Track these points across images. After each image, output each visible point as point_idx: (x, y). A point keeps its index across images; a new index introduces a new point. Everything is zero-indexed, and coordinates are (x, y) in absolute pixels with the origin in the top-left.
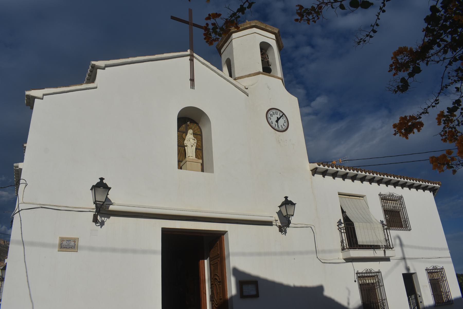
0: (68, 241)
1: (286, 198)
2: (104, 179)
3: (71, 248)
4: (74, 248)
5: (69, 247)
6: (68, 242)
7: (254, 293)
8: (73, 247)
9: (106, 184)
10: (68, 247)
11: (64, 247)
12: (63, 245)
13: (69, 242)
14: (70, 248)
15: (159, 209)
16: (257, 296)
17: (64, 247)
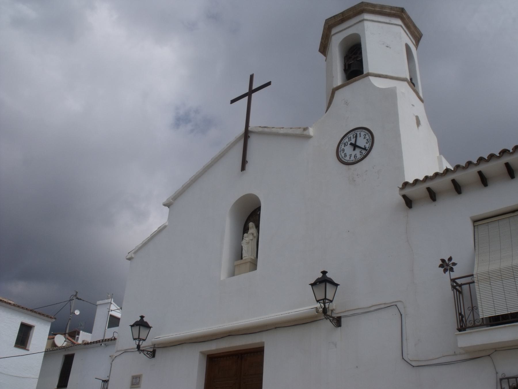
0: (136, 378)
2: (144, 317)
3: (137, 384)
4: (139, 383)
6: (136, 379)
9: (146, 323)
10: (136, 384)
11: (134, 384)
13: (137, 379)
17: (134, 384)
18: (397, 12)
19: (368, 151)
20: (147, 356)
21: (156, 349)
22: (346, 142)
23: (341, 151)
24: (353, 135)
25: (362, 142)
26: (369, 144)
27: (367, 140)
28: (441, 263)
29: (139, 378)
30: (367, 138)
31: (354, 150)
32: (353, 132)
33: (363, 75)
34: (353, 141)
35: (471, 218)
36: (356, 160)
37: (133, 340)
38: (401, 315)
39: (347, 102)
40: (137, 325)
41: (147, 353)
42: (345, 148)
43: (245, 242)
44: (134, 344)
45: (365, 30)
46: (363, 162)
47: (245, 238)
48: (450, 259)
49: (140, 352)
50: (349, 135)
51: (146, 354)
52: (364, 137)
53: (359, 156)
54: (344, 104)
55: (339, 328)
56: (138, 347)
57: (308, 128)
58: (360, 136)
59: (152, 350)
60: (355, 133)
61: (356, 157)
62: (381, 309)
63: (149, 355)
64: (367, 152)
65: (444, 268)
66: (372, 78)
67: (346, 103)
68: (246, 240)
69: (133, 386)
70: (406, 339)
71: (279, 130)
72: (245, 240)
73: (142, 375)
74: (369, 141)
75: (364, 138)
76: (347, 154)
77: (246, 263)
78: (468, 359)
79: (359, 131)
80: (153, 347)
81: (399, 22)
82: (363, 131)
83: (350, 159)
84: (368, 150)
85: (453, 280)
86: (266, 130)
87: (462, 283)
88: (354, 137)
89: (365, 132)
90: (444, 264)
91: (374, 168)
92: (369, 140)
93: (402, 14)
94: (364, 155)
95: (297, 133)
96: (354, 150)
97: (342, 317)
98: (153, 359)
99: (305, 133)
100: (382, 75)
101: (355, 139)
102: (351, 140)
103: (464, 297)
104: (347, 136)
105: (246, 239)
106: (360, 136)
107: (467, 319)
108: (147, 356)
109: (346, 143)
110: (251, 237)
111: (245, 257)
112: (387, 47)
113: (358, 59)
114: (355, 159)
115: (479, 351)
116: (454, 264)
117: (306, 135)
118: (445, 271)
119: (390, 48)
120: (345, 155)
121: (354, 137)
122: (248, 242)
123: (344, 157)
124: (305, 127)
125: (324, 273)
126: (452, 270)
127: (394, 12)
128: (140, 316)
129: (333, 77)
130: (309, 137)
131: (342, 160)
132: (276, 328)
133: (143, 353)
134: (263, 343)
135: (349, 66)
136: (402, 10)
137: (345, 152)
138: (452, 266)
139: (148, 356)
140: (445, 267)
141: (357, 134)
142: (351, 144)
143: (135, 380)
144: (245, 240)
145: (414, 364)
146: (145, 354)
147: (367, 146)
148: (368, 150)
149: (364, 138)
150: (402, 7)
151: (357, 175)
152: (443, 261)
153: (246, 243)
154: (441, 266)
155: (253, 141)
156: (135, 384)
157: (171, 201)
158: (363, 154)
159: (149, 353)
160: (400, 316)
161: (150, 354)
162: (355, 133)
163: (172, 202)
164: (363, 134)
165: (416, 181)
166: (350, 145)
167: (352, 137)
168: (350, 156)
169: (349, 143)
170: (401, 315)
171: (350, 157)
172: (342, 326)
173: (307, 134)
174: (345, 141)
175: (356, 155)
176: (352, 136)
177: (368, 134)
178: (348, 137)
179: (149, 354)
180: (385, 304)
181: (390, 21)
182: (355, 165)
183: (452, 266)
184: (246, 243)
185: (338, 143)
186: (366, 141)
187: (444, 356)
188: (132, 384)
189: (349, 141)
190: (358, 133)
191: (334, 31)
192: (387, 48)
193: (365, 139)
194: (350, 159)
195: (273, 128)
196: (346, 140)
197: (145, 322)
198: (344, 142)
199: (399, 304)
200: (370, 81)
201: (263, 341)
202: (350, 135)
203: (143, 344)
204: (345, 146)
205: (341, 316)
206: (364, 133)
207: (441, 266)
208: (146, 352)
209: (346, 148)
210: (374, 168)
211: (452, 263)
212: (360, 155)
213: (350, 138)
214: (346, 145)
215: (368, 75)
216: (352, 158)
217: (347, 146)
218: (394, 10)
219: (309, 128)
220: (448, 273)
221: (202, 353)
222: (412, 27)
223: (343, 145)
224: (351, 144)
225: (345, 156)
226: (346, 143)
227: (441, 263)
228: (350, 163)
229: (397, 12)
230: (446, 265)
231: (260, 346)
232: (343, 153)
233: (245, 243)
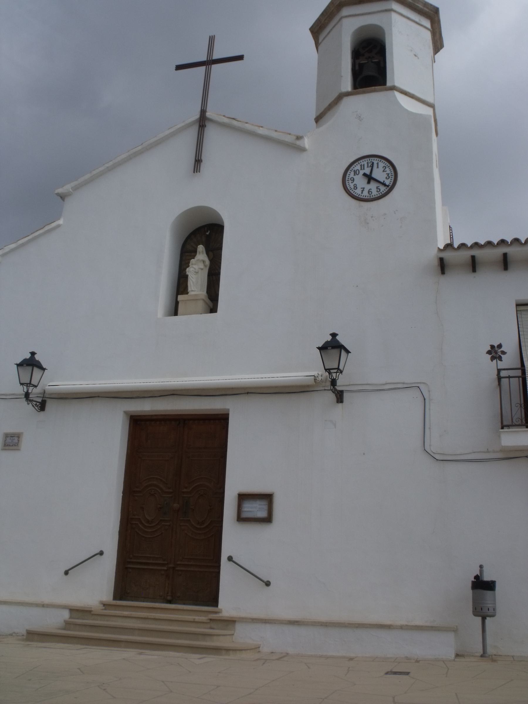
0: (12, 437)
1: (33, 354)
2: (36, 353)
3: (15, 445)
4: (17, 445)
5: (13, 444)
6: (12, 438)
7: (263, 514)
8: (16, 444)
9: (38, 362)
10: (11, 444)
11: (8, 445)
12: (6, 443)
13: (13, 438)
14: (13, 446)
15: (38, 396)
16: (268, 519)
17: (8, 445)
18: (430, 12)
19: (391, 188)
20: (35, 408)
21: (45, 399)
22: (357, 170)
23: (350, 179)
24: (368, 163)
25: (379, 174)
26: (389, 180)
27: (388, 174)
28: (489, 348)
29: (19, 437)
30: (387, 172)
31: (369, 182)
32: (368, 159)
33: (385, 86)
34: (367, 171)
35: (516, 301)
36: (370, 197)
37: (20, 385)
38: (425, 399)
39: (360, 117)
40: (28, 365)
41: (36, 405)
42: (355, 177)
43: (193, 271)
44: (21, 390)
45: (393, 26)
46: (381, 201)
47: (192, 264)
48: (500, 346)
49: (29, 403)
50: (361, 161)
51: (34, 405)
52: (383, 169)
53: (375, 193)
54: (356, 118)
55: (340, 404)
56: (27, 395)
57: (303, 137)
58: (378, 167)
59: (40, 400)
60: (371, 161)
61: (370, 193)
62: (399, 388)
63: (38, 408)
64: (388, 188)
65: (491, 355)
66: (397, 94)
67: (359, 118)
68: (195, 269)
69: (7, 448)
70: (430, 428)
71: (256, 128)
72: (193, 267)
73: (22, 433)
74: (390, 177)
75: (384, 171)
76: (357, 186)
77: (197, 300)
78: (505, 458)
79: (376, 160)
80: (42, 396)
81: (427, 23)
82: (382, 162)
83: (362, 193)
84: (390, 187)
85: (499, 371)
86: (235, 123)
87: (511, 375)
88: (369, 166)
89: (386, 164)
90: (492, 350)
91: (395, 214)
92: (390, 175)
93: (435, 16)
94: (383, 193)
95: (287, 140)
96: (369, 182)
97: (344, 391)
98: (42, 413)
99: (298, 143)
100: (409, 93)
101: (370, 169)
102: (364, 169)
103: (502, 389)
104: (359, 162)
105: (194, 266)
106: (378, 167)
107: (514, 416)
108: (35, 408)
109: (357, 171)
110: (201, 266)
111: (192, 291)
112: (415, 55)
113: (374, 61)
114: (369, 195)
115: (515, 450)
116: (504, 353)
117: (301, 146)
118: (493, 359)
119: (418, 58)
120: (355, 187)
121: (369, 166)
122: (196, 271)
123: (354, 188)
124: (300, 134)
125: (334, 335)
126: (500, 359)
127: (427, 10)
128: (30, 353)
129: (342, 77)
130: (302, 150)
131: (350, 192)
132: (248, 393)
133: (32, 404)
134: (228, 410)
135: (361, 66)
136: (436, 11)
137: (355, 183)
138: (501, 354)
139: (36, 408)
140: (493, 354)
141: (373, 163)
142: (365, 175)
143: (10, 439)
144: (193, 267)
145: (437, 457)
146: (33, 406)
147: (387, 182)
148: (390, 187)
149: (384, 171)
150: (436, 5)
151: (372, 217)
152: (492, 347)
153: (195, 272)
154: (489, 352)
155: (211, 131)
156: (10, 445)
157: (71, 190)
158: (381, 191)
159: (38, 404)
160: (424, 400)
161: (39, 406)
162: (371, 161)
163: (71, 192)
164: (381, 165)
165: (463, 246)
166: (363, 176)
167: (366, 166)
168: (362, 189)
169: (362, 172)
170: (425, 399)
171: (362, 191)
172: (344, 402)
173: (302, 145)
174: (356, 169)
175: (370, 191)
176: (365, 163)
177: (389, 166)
178: (360, 164)
179: (38, 406)
180: (404, 383)
181: (420, 20)
182: (372, 203)
183: (501, 355)
184: (195, 272)
185: (347, 167)
186: (386, 176)
187: (474, 452)
188: (5, 445)
189: (361, 169)
190: (375, 163)
191: (346, 11)
192: (414, 56)
193: (385, 173)
194: (362, 193)
195: (247, 123)
196: (357, 167)
197: (37, 360)
198: (354, 169)
199: (422, 387)
200: (395, 96)
201: (227, 407)
202: (363, 161)
203: (34, 392)
204: (355, 175)
205: (343, 390)
206: (384, 165)
207: (489, 352)
208: (35, 403)
209: (356, 177)
210: (395, 214)
211: (501, 351)
212: (377, 191)
213: (362, 166)
214: (358, 173)
215: (393, 88)
216: (365, 193)
217: (357, 175)
218: (427, 8)
219: (304, 137)
220: (495, 361)
221: (126, 413)
222: (438, 34)
223: (352, 173)
224: (365, 175)
225: (355, 188)
226: (357, 171)
227: (489, 348)
228: (362, 198)
229: (430, 12)
230: (494, 352)
231: (226, 413)
232: (352, 183)
233: (192, 271)
